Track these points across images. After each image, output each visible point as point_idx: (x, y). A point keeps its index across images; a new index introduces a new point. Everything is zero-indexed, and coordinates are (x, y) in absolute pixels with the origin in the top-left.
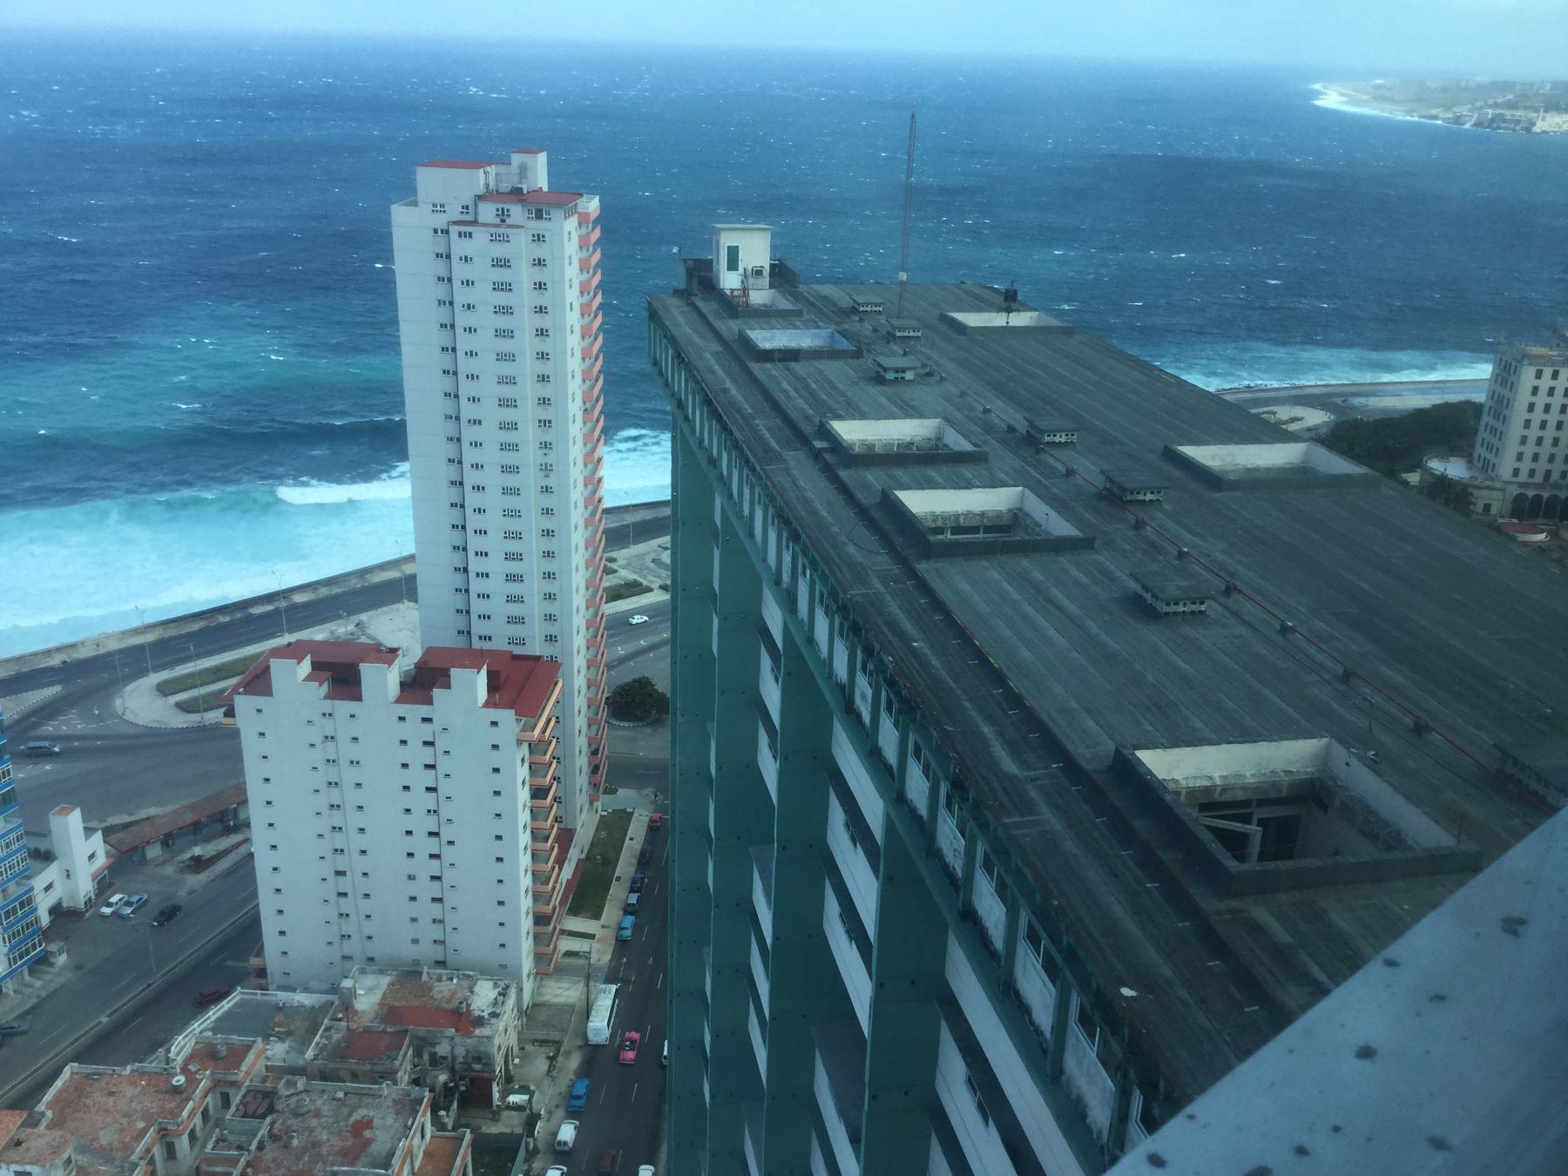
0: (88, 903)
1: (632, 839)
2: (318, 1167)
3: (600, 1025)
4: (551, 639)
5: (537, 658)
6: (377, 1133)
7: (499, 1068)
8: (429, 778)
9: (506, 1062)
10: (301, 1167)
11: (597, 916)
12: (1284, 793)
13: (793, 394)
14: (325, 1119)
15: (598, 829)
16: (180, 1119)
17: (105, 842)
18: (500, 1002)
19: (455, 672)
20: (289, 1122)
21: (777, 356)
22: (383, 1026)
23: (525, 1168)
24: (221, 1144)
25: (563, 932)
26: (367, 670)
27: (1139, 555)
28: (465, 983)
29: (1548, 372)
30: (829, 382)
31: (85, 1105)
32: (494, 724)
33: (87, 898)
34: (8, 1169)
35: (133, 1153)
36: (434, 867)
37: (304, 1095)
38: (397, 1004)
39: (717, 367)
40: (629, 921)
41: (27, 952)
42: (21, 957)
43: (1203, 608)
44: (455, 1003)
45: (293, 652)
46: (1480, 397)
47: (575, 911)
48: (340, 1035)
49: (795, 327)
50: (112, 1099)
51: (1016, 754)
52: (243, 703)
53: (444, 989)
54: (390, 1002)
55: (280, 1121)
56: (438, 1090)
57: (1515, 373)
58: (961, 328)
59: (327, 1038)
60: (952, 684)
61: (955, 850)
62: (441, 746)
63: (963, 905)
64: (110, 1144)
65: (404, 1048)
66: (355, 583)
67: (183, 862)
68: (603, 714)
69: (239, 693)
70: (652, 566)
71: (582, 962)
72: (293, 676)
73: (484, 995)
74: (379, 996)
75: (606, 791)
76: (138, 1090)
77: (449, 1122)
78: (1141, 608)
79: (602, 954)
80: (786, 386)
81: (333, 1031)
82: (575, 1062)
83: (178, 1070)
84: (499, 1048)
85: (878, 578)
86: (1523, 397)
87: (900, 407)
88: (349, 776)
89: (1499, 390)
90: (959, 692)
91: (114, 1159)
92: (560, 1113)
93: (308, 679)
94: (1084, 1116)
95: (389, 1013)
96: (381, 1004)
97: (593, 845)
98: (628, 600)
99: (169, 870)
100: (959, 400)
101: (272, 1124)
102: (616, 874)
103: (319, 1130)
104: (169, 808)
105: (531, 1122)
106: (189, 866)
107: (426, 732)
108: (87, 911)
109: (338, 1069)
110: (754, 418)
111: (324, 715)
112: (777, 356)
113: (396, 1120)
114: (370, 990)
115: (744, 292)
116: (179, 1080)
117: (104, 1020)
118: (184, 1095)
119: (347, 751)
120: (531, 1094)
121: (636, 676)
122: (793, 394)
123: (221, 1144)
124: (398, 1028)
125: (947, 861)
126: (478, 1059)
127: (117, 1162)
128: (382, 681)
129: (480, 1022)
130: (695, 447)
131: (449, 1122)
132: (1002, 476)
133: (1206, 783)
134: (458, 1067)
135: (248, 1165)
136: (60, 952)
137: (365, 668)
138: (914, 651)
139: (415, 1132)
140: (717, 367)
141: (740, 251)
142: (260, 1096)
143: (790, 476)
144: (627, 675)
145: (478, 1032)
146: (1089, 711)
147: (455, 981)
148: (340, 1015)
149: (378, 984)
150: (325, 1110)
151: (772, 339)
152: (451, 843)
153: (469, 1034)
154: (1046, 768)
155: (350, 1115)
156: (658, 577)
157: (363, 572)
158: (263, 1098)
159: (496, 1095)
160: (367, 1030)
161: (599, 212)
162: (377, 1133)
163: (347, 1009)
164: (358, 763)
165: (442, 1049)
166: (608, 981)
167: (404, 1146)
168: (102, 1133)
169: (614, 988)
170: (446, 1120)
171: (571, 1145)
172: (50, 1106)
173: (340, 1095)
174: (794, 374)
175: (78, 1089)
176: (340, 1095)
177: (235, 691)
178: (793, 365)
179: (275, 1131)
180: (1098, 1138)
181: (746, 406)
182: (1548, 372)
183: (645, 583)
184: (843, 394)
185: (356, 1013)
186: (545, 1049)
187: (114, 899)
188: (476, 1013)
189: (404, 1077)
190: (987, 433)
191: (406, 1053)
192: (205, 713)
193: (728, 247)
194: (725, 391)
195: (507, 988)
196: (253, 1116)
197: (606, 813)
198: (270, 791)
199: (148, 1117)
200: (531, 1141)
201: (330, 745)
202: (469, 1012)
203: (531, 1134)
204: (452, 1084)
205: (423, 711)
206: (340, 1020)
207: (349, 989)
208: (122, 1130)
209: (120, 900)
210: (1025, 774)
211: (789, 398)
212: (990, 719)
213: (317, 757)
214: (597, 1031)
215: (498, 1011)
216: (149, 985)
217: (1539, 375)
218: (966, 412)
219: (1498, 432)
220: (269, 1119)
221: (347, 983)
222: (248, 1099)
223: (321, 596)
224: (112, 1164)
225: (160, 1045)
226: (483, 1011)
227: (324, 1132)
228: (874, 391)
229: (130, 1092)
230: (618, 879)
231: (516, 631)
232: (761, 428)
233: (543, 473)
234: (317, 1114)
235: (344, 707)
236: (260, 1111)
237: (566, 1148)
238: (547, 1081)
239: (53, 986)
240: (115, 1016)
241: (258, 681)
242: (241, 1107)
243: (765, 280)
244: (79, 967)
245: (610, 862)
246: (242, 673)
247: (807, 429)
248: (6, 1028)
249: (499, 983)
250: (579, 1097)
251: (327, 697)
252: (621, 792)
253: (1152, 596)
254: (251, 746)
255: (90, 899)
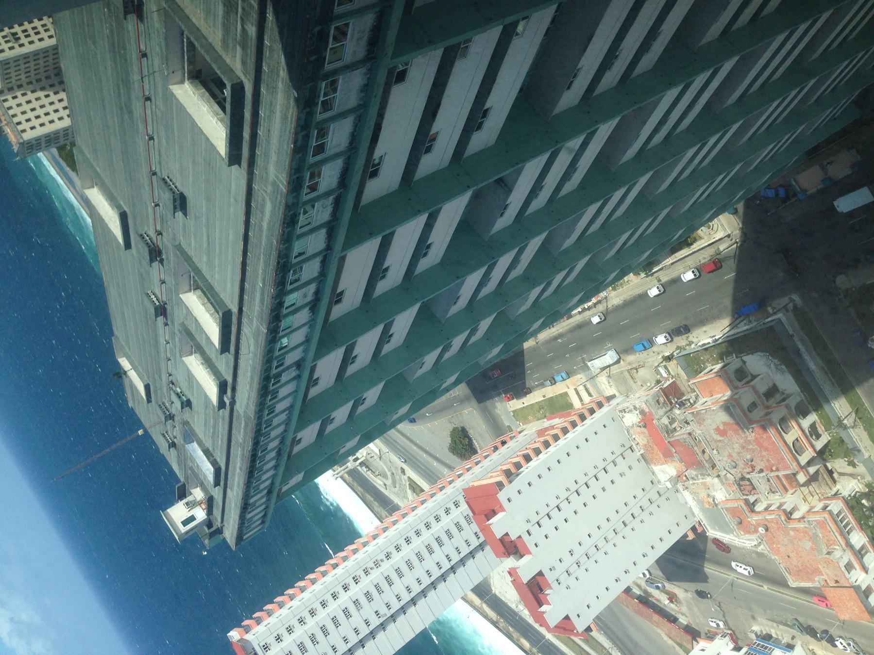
0: (724, 636)
1: (523, 403)
2: (751, 438)
3: (610, 357)
4: (457, 505)
5: (467, 503)
6: (718, 423)
7: (656, 389)
8: (555, 513)
9: (652, 389)
10: (756, 446)
11: (566, 394)
12: (204, 90)
13: (220, 436)
14: (730, 451)
15: (530, 422)
16: (777, 517)
17: (693, 649)
18: (628, 409)
19: (499, 536)
20: (742, 466)
21: (211, 459)
22: (675, 455)
23: (687, 347)
24: (773, 490)
25: (583, 404)
26: (525, 578)
27: (169, 223)
28: (631, 431)
29: (20, 128)
30: (205, 424)
31: (802, 565)
32: (509, 500)
33: (722, 638)
34: (850, 578)
35: (806, 527)
36: (592, 482)
37: (727, 468)
38: (661, 456)
39: (236, 484)
40: (558, 378)
41: (763, 646)
42: (766, 647)
43: (166, 178)
44: (643, 429)
45: (540, 618)
46: (54, 151)
47: (570, 406)
48: (692, 471)
49: (198, 466)
50: (791, 555)
51: (263, 206)
52: (580, 626)
53: (641, 438)
54: (663, 459)
55: (745, 470)
56: (683, 411)
57: (31, 142)
58: (147, 387)
59: (697, 477)
60: (262, 256)
61: (324, 208)
62: (536, 518)
63: (340, 189)
64: (809, 541)
65: (677, 438)
66: (502, 623)
67: (676, 605)
68: (475, 458)
69: (577, 631)
70: (397, 486)
71: (588, 385)
72: (553, 612)
73: (632, 419)
74: (664, 466)
75: (510, 430)
76: (779, 546)
77: (693, 395)
78: (181, 203)
79: (580, 378)
80: (220, 442)
81: (693, 476)
82: (631, 358)
83: (758, 534)
84: (647, 395)
85: (252, 325)
86: (39, 132)
87: (193, 383)
88: (579, 552)
89: (43, 145)
90: (262, 251)
91: (813, 534)
92: (655, 349)
93: (549, 604)
94: (366, 85)
95: (667, 455)
96: (666, 462)
97: (538, 419)
98: (421, 485)
99: (684, 609)
100: (172, 359)
101: (748, 473)
102: (543, 399)
103: (736, 450)
104: (659, 631)
105: (669, 358)
106: (676, 601)
107: (534, 529)
108: (728, 634)
109: (706, 461)
110: (241, 444)
111: (559, 584)
112: (211, 459)
113: (707, 419)
114: (664, 472)
115: (201, 503)
116: (761, 530)
117: (765, 587)
118: (766, 523)
119: (569, 560)
120: (656, 367)
121: (451, 454)
122: (220, 436)
123: (773, 490)
124: (671, 447)
125: (332, 209)
126: (658, 401)
127: (814, 531)
128: (527, 568)
129: (642, 412)
130: (282, 469)
131: (693, 395)
132: (184, 312)
133: (219, 122)
134: (668, 409)
135: (772, 471)
136: (752, 631)
137: (525, 580)
138: (264, 284)
139: (706, 406)
140: (236, 484)
141: (183, 520)
142: (742, 488)
143: (248, 404)
144: (452, 459)
145: (647, 410)
146: (230, 192)
147: (634, 437)
148: (684, 478)
149: (660, 471)
150: (726, 454)
151: (208, 470)
152: (576, 482)
153: (650, 413)
154: (259, 190)
155: (720, 441)
156: (400, 479)
157: (495, 624)
158: (742, 486)
159: (668, 383)
160: (681, 461)
161: (235, 629)
162: (718, 423)
163: (679, 476)
164: (570, 552)
165: (665, 421)
166: (589, 368)
167: (714, 407)
168: (808, 548)
169: (589, 364)
170: (694, 397)
171: (665, 334)
172: (813, 581)
173: (715, 451)
174: (214, 444)
175: (798, 573)
176: (715, 451)
177: (577, 634)
178: (211, 449)
179: (750, 469)
180: (368, 74)
181: (239, 453)
182: (20, 128)
183: (408, 483)
184: (206, 414)
185: (678, 471)
186: (635, 375)
187: (714, 625)
188: (640, 416)
189: (689, 429)
190: (175, 333)
191: (678, 436)
192: (607, 648)
193: (184, 526)
194: (241, 469)
195: (621, 411)
196: (752, 484)
197: (521, 424)
198: (611, 584)
199: (786, 534)
200: (675, 354)
201: (571, 570)
202: (642, 420)
203: (672, 355)
204: (677, 405)
205: (525, 537)
206: (686, 476)
207: (670, 482)
208: (800, 540)
209: (712, 622)
210: (266, 197)
211: (222, 436)
212: (261, 227)
213: (581, 573)
214: (611, 357)
215: (633, 407)
216: (737, 578)
217: (24, 131)
218: (174, 351)
219: (64, 133)
220: (748, 476)
221: (669, 485)
222: (747, 493)
223: (519, 634)
224: (816, 533)
225: (757, 553)
226: (637, 414)
227: (735, 447)
228: (194, 402)
229: (782, 549)
230: (544, 396)
231: (463, 523)
232: (242, 437)
233: (381, 563)
234: (730, 456)
235: (550, 577)
236: (748, 483)
237: (667, 335)
238: (647, 365)
239: (770, 623)
240: (761, 584)
241: (565, 626)
242: (752, 493)
243: (190, 498)
244: (753, 618)
245: (540, 406)
246: (569, 637)
247: (226, 412)
248: (800, 630)
249: (621, 416)
250: (643, 345)
251: (551, 588)
252: (507, 424)
253: (176, 202)
254: (598, 608)
255: (722, 636)
